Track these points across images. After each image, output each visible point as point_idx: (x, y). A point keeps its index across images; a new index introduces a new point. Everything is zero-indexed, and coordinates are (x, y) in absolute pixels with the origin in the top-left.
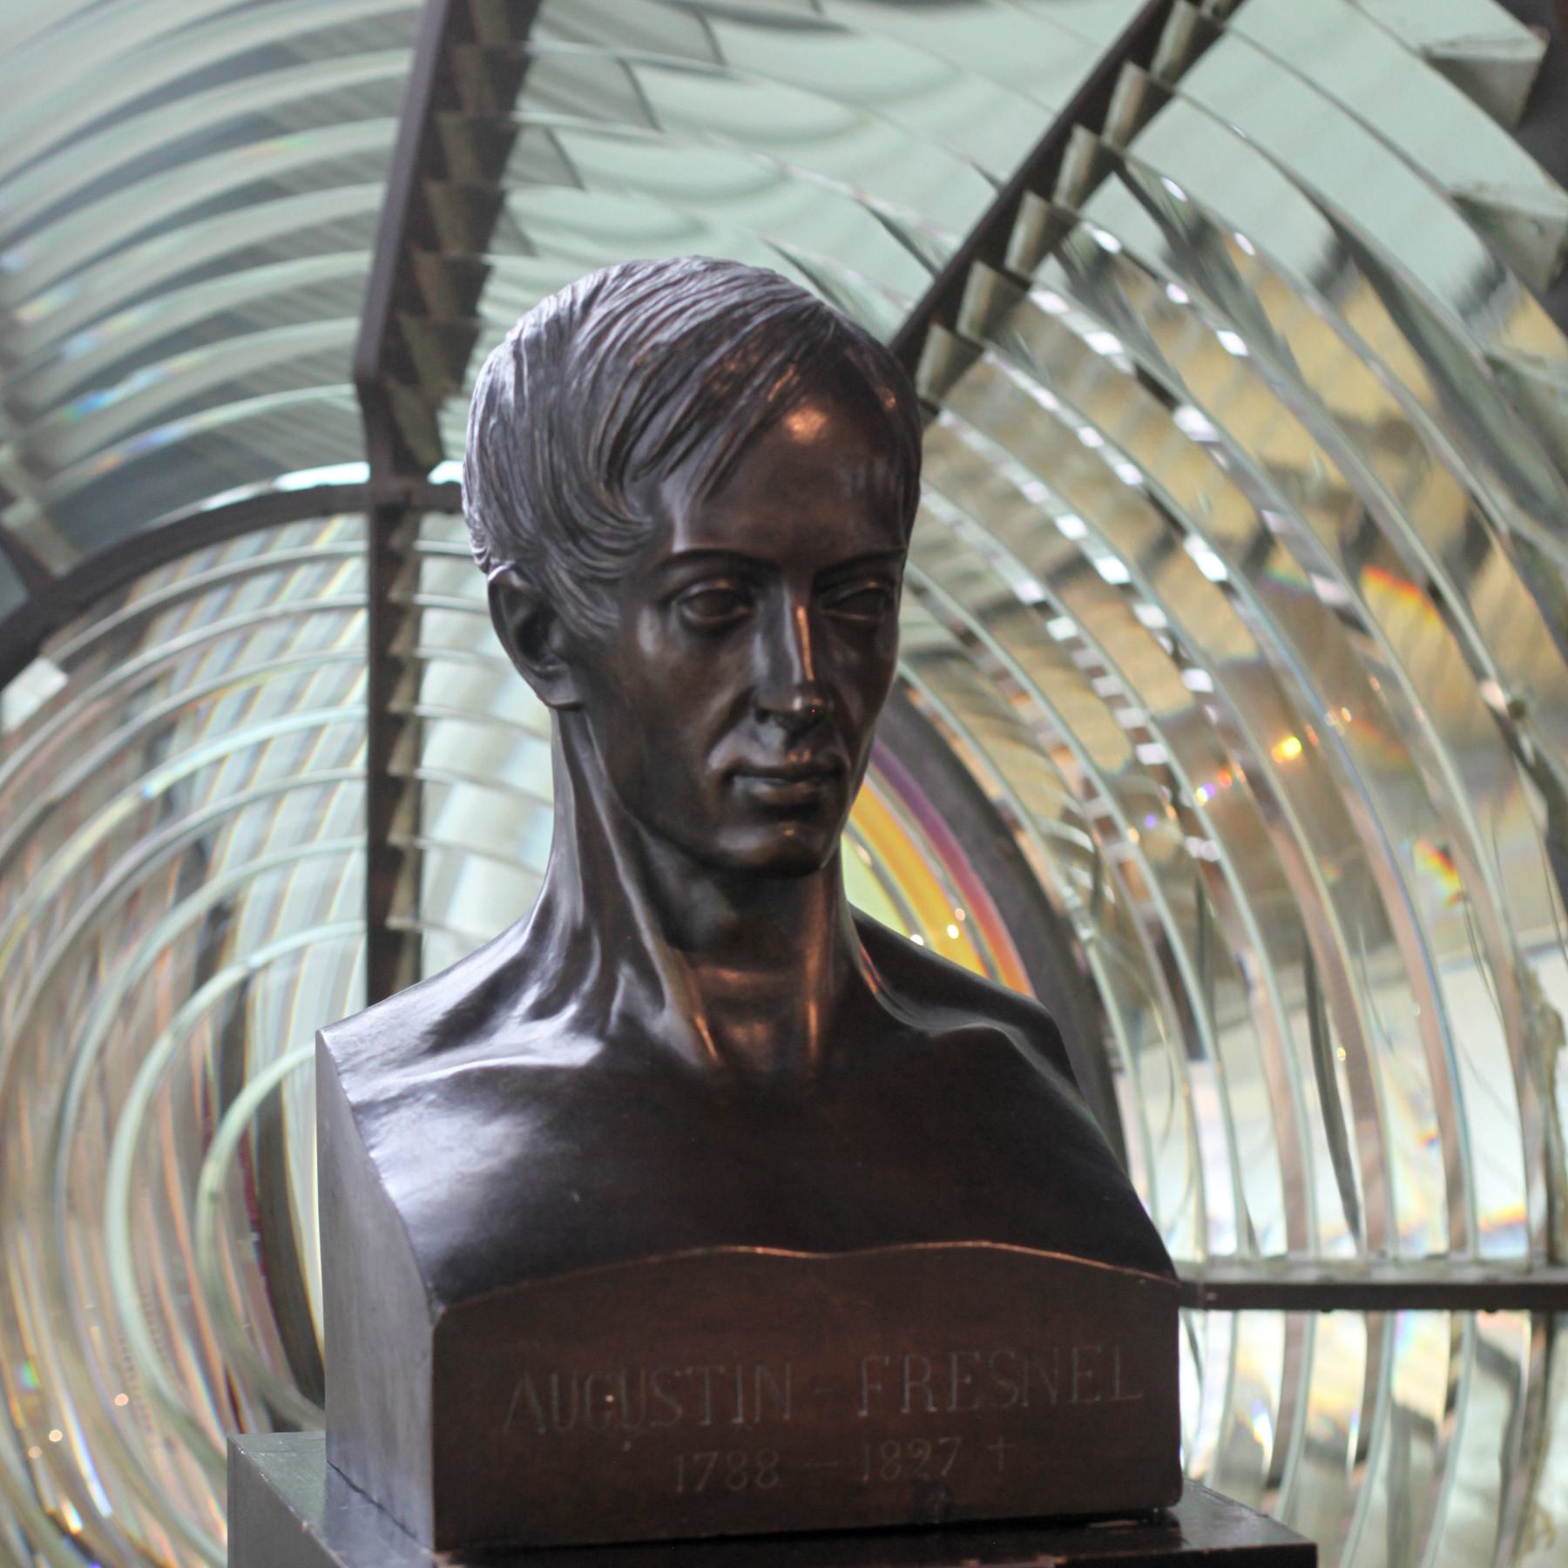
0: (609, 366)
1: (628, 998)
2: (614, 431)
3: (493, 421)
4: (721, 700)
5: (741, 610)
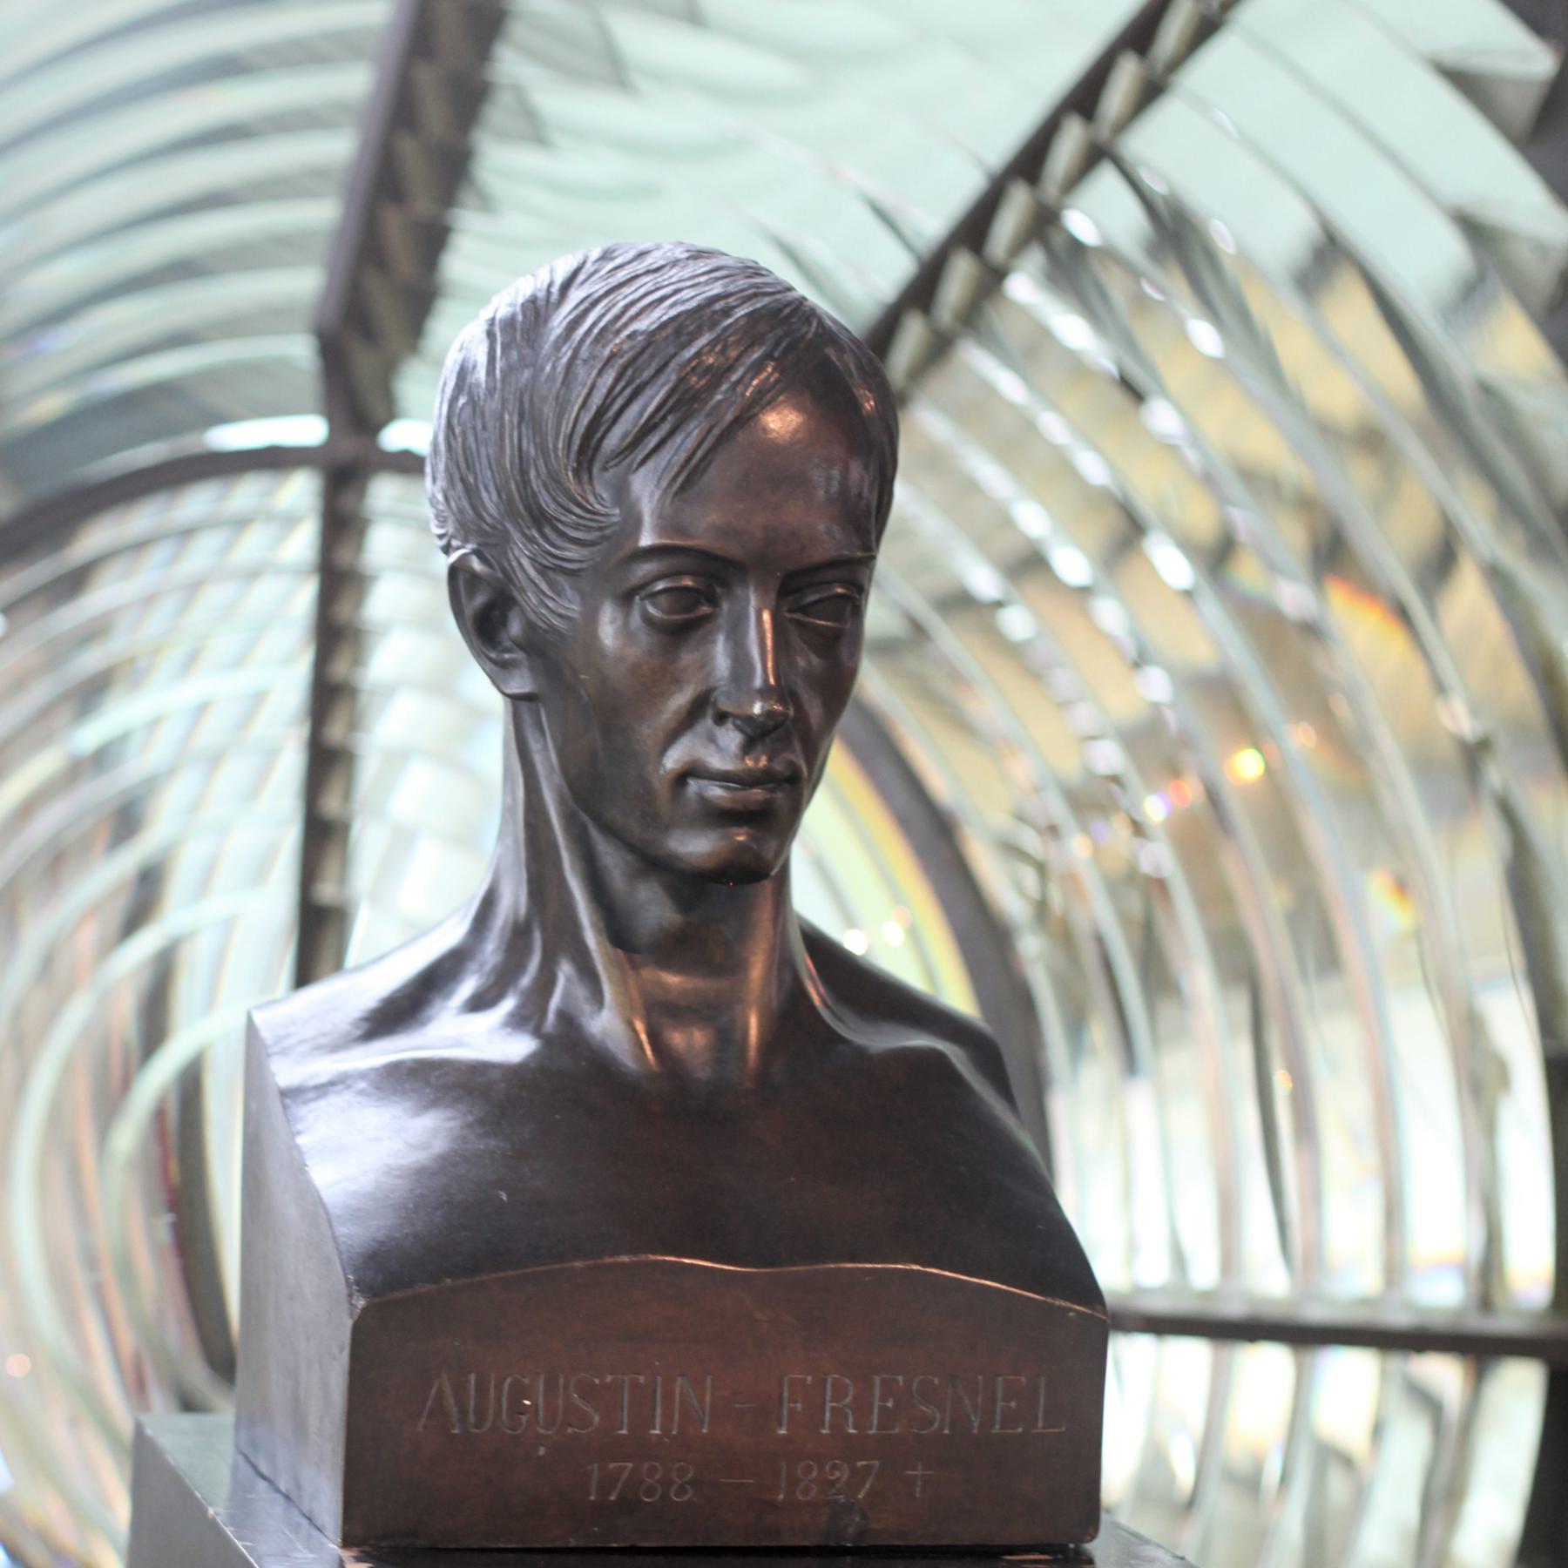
1: (567, 995)
2: (585, 420)
3: (462, 400)
4: (680, 700)
5: (705, 609)
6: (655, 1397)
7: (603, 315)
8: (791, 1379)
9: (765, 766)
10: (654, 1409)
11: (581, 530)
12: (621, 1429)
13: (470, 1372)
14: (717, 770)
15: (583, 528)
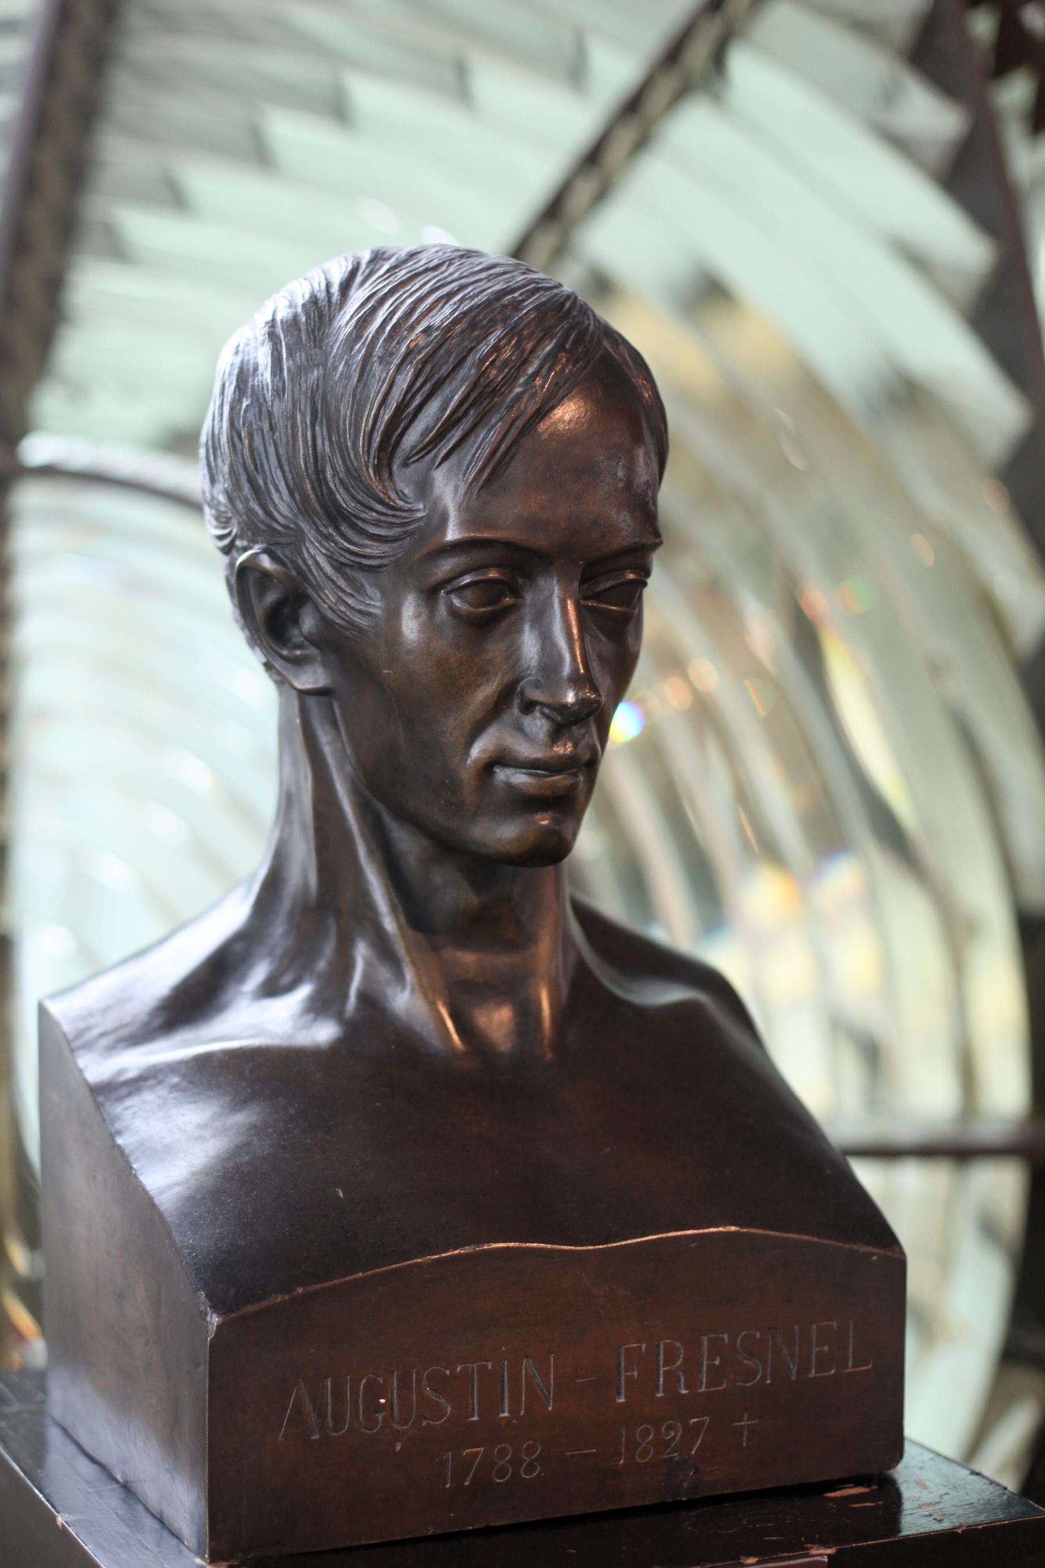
0: (378, 350)
1: (366, 977)
2: (387, 415)
3: (245, 403)
4: (487, 691)
5: (508, 600)
6: (503, 1381)
7: (392, 313)
8: (627, 1349)
9: (571, 751)
10: (503, 1393)
11: (381, 526)
12: (473, 1416)
13: (327, 1377)
14: (526, 758)
15: (385, 525)
